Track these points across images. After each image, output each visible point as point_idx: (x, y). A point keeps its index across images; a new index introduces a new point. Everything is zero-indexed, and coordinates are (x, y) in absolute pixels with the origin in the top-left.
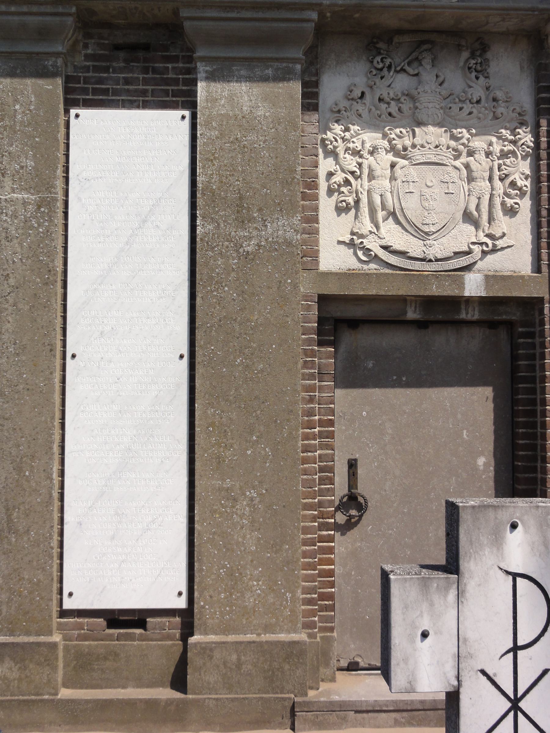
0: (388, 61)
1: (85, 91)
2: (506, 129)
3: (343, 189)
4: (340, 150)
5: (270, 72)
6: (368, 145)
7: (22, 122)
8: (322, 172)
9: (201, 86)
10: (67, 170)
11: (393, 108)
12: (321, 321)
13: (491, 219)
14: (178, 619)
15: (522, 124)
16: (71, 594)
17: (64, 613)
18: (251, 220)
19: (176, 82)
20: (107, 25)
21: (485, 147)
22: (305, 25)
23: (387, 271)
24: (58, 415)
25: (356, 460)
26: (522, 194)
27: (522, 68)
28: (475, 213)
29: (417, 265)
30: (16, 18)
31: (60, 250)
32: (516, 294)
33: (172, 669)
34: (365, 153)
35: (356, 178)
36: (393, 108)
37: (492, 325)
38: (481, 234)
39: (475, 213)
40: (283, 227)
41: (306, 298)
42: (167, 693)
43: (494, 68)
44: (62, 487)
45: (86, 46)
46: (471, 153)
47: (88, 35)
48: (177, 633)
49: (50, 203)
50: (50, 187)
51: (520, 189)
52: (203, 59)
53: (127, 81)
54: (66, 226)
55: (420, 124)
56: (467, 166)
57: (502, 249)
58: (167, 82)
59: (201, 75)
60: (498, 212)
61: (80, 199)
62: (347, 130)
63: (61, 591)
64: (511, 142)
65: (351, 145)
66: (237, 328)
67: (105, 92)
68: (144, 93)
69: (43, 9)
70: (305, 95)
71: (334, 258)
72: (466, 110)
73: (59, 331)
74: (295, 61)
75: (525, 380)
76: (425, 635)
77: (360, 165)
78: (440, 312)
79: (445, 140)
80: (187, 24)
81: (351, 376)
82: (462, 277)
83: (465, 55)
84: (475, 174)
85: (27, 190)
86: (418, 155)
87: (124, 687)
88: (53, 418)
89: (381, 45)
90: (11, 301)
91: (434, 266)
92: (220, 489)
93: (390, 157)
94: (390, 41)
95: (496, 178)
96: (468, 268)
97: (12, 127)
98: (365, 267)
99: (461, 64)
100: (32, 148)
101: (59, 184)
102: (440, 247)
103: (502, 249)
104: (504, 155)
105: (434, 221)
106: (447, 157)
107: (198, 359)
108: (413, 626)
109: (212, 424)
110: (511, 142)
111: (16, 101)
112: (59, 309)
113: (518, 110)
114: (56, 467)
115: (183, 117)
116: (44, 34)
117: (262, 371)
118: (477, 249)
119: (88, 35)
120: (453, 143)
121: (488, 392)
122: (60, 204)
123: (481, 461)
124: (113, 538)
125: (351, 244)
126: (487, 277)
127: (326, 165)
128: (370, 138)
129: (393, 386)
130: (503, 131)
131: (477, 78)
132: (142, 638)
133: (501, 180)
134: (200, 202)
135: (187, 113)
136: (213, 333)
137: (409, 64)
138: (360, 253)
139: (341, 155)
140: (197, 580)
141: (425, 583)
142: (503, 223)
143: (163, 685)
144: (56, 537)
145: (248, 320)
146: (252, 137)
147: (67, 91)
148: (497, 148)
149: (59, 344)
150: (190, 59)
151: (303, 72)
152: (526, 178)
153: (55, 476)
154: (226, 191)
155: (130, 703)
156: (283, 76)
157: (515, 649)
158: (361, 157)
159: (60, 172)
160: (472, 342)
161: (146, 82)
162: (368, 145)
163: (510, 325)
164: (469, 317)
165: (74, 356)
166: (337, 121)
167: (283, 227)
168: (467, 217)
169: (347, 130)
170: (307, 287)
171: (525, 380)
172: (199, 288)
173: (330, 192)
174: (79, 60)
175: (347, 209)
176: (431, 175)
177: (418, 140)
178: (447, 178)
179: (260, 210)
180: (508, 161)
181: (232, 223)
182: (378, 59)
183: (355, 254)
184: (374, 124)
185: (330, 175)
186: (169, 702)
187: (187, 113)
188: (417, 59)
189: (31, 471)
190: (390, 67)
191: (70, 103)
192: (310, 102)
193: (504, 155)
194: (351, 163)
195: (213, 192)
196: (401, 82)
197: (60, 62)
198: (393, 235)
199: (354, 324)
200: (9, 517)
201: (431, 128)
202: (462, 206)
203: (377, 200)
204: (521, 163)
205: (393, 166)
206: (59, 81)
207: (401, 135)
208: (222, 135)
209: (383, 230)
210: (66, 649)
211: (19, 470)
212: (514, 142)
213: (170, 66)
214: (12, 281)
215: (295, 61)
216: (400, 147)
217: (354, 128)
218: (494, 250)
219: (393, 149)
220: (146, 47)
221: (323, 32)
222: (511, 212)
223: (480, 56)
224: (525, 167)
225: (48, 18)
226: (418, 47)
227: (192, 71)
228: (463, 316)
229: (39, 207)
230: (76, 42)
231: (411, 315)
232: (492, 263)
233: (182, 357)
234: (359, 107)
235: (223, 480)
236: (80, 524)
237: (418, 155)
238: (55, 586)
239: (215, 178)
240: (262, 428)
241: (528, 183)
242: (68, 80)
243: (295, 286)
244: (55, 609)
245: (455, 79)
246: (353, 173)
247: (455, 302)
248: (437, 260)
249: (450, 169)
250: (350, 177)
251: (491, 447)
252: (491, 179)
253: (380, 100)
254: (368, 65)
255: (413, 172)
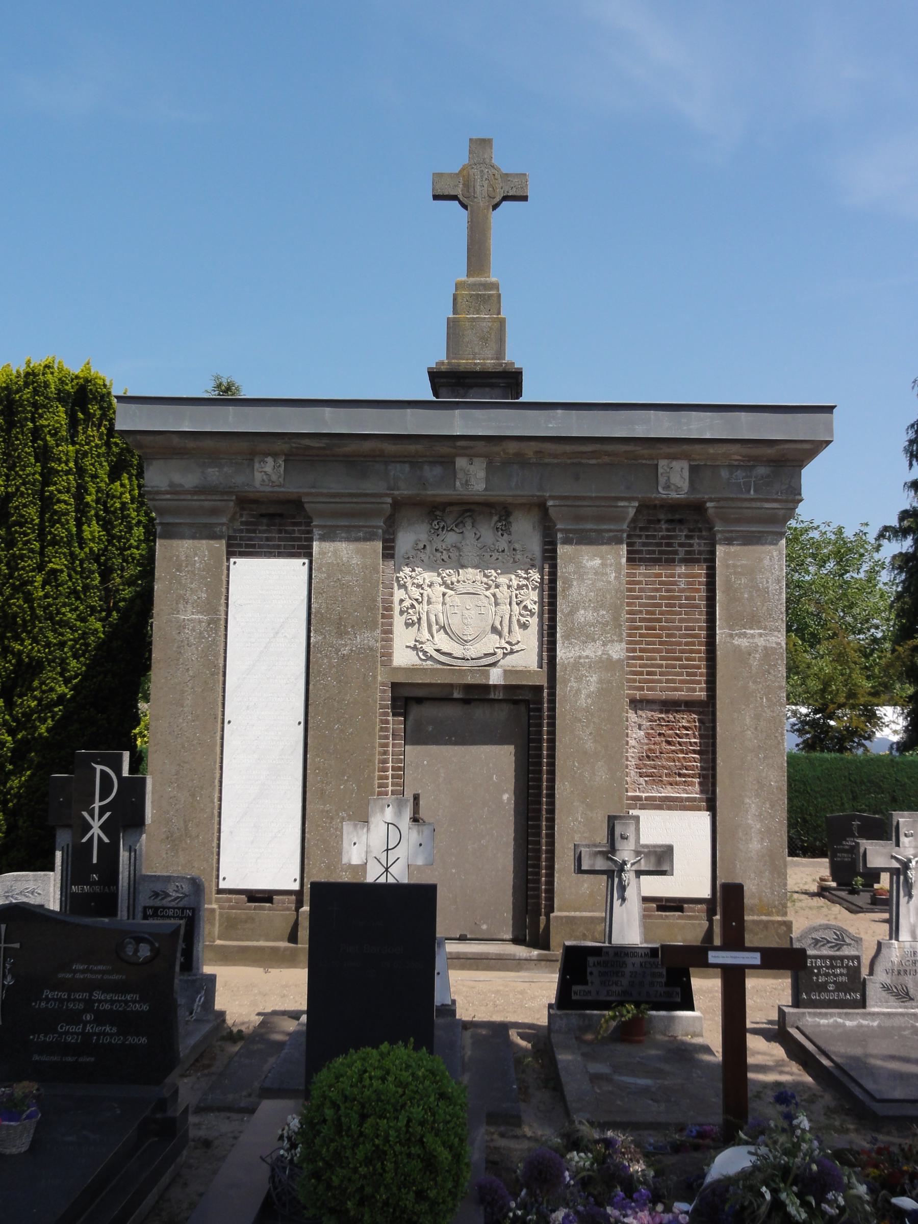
0: (442, 524)
1: (240, 546)
2: (521, 569)
3: (410, 611)
4: (409, 585)
5: (361, 534)
6: (427, 582)
7: (199, 569)
8: (396, 599)
9: (315, 544)
10: (227, 599)
11: (445, 557)
12: (394, 699)
13: (510, 632)
14: (294, 897)
15: (533, 566)
16: (224, 879)
17: (220, 891)
18: (347, 633)
19: (300, 539)
20: (256, 502)
21: (507, 582)
22: (384, 506)
23: (439, 666)
24: (218, 760)
25: (418, 795)
26: (532, 614)
27: (534, 527)
28: (499, 627)
29: (459, 662)
30: (198, 503)
31: (222, 652)
32: (524, 683)
33: (289, 930)
34: (426, 588)
35: (419, 603)
36: (445, 557)
37: (516, 702)
38: (503, 641)
39: (499, 627)
40: (368, 638)
41: (383, 684)
42: (284, 944)
43: (514, 528)
44: (220, 808)
45: (241, 516)
46: (497, 586)
47: (243, 509)
48: (293, 906)
49: (215, 622)
50: (216, 611)
51: (530, 611)
52: (317, 526)
53: (268, 539)
54: (226, 635)
55: (463, 566)
56: (494, 595)
57: (517, 651)
58: (294, 539)
59: (316, 537)
60: (515, 626)
61: (235, 618)
62: (413, 570)
63: (218, 877)
64: (525, 578)
65: (416, 581)
66: (336, 704)
67: (254, 546)
68: (279, 547)
69: (214, 497)
70: (384, 548)
71: (403, 657)
72: (494, 558)
73: (220, 704)
74: (378, 527)
75: (534, 741)
76: (355, 844)
77: (422, 594)
78: (476, 694)
79: (479, 577)
80: (306, 506)
81: (416, 735)
82: (488, 671)
83: (495, 518)
84: (499, 601)
85: (202, 613)
86: (461, 588)
87: (257, 941)
88: (215, 762)
89: (438, 513)
90: (190, 686)
91: (471, 663)
92: (322, 811)
93: (443, 589)
94: (443, 511)
95: (514, 603)
96: (494, 665)
97: (193, 572)
98: (424, 663)
99: (492, 525)
100: (205, 585)
101: (222, 608)
102: (474, 650)
103: (517, 651)
104: (520, 587)
105: (470, 632)
106: (480, 588)
107: (310, 725)
108: (351, 840)
109: (318, 768)
110: (525, 578)
111: (196, 555)
112: (220, 690)
113: (530, 556)
114: (217, 795)
115: (304, 564)
116: (214, 512)
117: (352, 733)
118: (499, 651)
119: (243, 509)
120: (485, 580)
121: (511, 748)
122: (222, 622)
123: (505, 797)
124: (252, 842)
125: (415, 648)
126: (505, 671)
127: (398, 594)
128: (429, 576)
129: (446, 744)
130: (519, 571)
131: (502, 535)
132: (270, 909)
133: (518, 604)
134: (313, 621)
135: (306, 561)
136: (320, 708)
137: (456, 526)
138: (421, 654)
139: (409, 588)
140: (306, 870)
141: (355, 826)
142: (518, 634)
143: (282, 940)
144: (216, 841)
145: (344, 700)
146: (348, 578)
147: (229, 546)
148: (515, 583)
149: (220, 714)
150: (308, 524)
151: (384, 532)
152: (535, 603)
153: (216, 800)
154: (331, 614)
155: (262, 949)
156: (370, 538)
157: (387, 850)
158: (423, 589)
159: (223, 601)
160: (502, 713)
161: (280, 539)
162: (427, 582)
163: (527, 702)
164: (496, 697)
165: (229, 722)
166: (407, 565)
167: (368, 638)
168: (494, 630)
169: (413, 570)
170: (382, 677)
171: (534, 741)
172: (311, 678)
173: (402, 613)
174: (237, 525)
175: (413, 624)
176: (469, 601)
177: (461, 578)
178: (480, 604)
179: (353, 627)
180: (522, 592)
181: (335, 631)
182: (436, 522)
183: (418, 654)
184: (432, 567)
185: (402, 601)
186: (286, 949)
187: (306, 561)
188: (462, 522)
189: (201, 797)
190: (443, 528)
191: (230, 554)
192: (389, 553)
193: (520, 587)
194: (415, 592)
195: (322, 614)
196: (451, 538)
197: (224, 528)
198: (443, 642)
199: (419, 701)
200: (186, 826)
201: (470, 570)
202: (491, 623)
203: (433, 619)
204: (532, 592)
205: (444, 595)
206: (224, 542)
207: (449, 574)
208: (329, 577)
209: (436, 638)
210: (221, 915)
211: (193, 796)
212: (527, 579)
213: (296, 528)
214: (191, 673)
215: (378, 527)
216: (449, 582)
217: (418, 570)
218: (512, 652)
219: (444, 583)
220: (281, 515)
221: (398, 505)
222: (524, 626)
223: (505, 520)
224: (534, 595)
225: (219, 503)
226: (463, 514)
227: (310, 532)
228: (492, 696)
229: (209, 624)
230: (235, 513)
231: (456, 695)
232: (511, 661)
233: (300, 723)
234: (422, 556)
235: (325, 805)
236: (231, 832)
237: (461, 588)
238: (215, 873)
239: (324, 605)
240: (351, 772)
241: (536, 607)
242: (230, 538)
243: (375, 677)
244: (214, 888)
245: (487, 533)
246: (417, 600)
247: (487, 688)
248: (472, 659)
249: (482, 597)
250: (415, 603)
251: (513, 788)
252: (510, 604)
253: (436, 550)
254: (429, 526)
255: (457, 599)
